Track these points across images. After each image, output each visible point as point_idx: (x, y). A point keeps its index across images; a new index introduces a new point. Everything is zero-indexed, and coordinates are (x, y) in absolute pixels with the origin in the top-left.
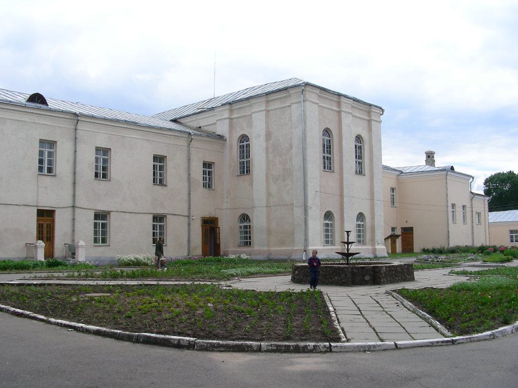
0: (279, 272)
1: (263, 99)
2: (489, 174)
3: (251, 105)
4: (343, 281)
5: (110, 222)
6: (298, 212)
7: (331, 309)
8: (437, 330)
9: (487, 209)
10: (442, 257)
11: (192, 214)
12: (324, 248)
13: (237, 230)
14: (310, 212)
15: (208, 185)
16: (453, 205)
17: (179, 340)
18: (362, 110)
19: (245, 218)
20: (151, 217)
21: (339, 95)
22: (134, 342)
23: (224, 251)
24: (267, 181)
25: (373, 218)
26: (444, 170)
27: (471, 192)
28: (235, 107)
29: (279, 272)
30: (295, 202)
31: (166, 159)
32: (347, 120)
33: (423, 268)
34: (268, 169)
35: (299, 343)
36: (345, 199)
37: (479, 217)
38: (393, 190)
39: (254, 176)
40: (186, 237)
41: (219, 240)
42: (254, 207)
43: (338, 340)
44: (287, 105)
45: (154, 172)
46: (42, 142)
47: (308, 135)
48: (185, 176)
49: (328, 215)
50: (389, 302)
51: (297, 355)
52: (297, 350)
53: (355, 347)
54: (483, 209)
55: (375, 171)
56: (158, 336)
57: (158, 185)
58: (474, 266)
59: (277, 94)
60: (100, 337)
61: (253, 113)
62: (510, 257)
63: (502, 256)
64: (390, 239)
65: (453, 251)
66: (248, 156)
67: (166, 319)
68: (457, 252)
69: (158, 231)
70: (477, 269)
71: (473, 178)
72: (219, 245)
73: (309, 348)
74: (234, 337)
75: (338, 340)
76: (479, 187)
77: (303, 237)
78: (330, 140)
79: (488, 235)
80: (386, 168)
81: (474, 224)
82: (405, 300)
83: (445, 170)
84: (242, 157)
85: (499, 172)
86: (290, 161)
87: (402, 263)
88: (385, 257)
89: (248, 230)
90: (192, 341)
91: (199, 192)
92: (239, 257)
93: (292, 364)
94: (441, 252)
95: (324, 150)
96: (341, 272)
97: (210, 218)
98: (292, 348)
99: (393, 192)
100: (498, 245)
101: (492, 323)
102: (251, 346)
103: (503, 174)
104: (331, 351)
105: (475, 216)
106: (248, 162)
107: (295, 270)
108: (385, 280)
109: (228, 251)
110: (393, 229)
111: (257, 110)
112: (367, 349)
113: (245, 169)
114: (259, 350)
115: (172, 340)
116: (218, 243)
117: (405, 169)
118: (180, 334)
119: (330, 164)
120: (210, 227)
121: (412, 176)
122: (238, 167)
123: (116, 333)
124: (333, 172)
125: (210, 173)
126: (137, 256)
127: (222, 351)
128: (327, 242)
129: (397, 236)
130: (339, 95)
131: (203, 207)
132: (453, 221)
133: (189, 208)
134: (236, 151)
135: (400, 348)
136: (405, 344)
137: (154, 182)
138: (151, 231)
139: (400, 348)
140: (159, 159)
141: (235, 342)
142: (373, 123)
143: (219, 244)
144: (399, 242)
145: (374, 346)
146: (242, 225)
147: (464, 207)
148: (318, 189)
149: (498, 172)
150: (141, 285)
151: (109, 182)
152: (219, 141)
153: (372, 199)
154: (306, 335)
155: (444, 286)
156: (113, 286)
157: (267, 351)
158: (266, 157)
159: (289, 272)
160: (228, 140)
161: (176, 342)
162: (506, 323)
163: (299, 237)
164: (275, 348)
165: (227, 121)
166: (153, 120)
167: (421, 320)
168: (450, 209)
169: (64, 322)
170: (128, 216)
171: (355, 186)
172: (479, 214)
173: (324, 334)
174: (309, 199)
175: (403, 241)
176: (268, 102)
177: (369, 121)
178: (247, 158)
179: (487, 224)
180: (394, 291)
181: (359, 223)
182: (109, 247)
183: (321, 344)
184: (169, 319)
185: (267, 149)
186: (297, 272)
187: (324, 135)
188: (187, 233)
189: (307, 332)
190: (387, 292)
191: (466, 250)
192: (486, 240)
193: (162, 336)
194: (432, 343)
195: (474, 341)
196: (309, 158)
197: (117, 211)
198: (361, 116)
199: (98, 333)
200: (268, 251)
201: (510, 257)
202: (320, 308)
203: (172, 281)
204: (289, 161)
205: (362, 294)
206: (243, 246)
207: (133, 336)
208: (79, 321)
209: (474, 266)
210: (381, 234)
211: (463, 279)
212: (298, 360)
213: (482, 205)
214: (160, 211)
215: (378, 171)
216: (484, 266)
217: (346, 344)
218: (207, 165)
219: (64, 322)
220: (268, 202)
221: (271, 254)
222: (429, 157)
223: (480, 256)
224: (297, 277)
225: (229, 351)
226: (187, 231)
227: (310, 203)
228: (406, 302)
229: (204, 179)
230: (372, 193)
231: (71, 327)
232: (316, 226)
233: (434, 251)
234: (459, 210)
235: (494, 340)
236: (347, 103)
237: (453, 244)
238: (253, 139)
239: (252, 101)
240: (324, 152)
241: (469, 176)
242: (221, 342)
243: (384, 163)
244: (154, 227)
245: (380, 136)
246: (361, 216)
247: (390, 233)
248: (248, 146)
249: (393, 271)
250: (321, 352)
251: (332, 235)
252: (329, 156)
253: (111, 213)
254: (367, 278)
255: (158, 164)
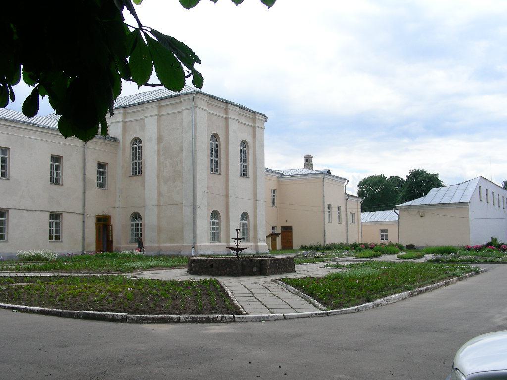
0: (175, 266)
1: (156, 105)
2: (362, 178)
3: (144, 110)
4: (234, 272)
5: (8, 218)
6: (187, 211)
7: (229, 292)
8: (315, 306)
9: (360, 210)
10: (319, 254)
11: (87, 211)
12: (210, 244)
13: (129, 228)
14: (198, 211)
15: (102, 184)
16: (329, 206)
17: (114, 315)
18: (247, 117)
19: (136, 216)
20: (48, 214)
21: (227, 103)
22: (75, 318)
23: (116, 247)
24: (159, 182)
25: (256, 217)
26: (321, 173)
27: (346, 194)
28: (129, 110)
29: (175, 266)
30: (184, 202)
31: (63, 158)
32: (233, 126)
33: (302, 263)
34: (159, 170)
35: (210, 316)
36: (231, 200)
37: (352, 217)
38: (274, 191)
39: (146, 176)
40: (81, 234)
41: (112, 237)
42: (145, 206)
43: (240, 313)
44: (179, 110)
45: (51, 172)
46: (382, 231)
47: (198, 140)
48: (81, 176)
49: (215, 214)
50: (273, 287)
51: (209, 324)
52: (208, 320)
53: (253, 318)
54: (356, 210)
55: (258, 174)
56: (96, 312)
57: (55, 184)
58: (347, 261)
59: (169, 100)
60: (44, 316)
61: (146, 117)
62: (379, 253)
63: (372, 252)
64: (271, 237)
65: (328, 248)
66: (140, 158)
67: (95, 301)
68: (333, 249)
69: (54, 228)
70: (349, 263)
71: (348, 181)
72: (112, 242)
73: (218, 319)
74: (158, 312)
75: (240, 313)
76: (353, 189)
77: (191, 235)
78: (217, 145)
79: (360, 233)
80: (268, 170)
81: (348, 223)
82: (288, 286)
83: (323, 173)
84: (134, 158)
85: (372, 175)
86: (181, 163)
87: (285, 257)
88: (267, 254)
89: (139, 227)
90: (124, 316)
91: (94, 191)
92: (132, 253)
93: (206, 329)
94: (318, 249)
95: (212, 154)
96: (232, 264)
97: (103, 216)
98: (204, 319)
99: (274, 193)
100: (369, 242)
101: (358, 301)
102: (172, 318)
103: (376, 177)
104: (234, 321)
105: (350, 217)
106: (140, 164)
107: (191, 263)
108: (270, 271)
109: (120, 247)
110: (274, 228)
111: (149, 115)
112: (262, 319)
113: (137, 170)
114: (179, 321)
115: (107, 316)
116: (111, 239)
117: (285, 172)
118: (112, 311)
119: (217, 167)
120: (103, 224)
121: (292, 178)
122: (130, 168)
123: (59, 312)
124: (220, 174)
125: (103, 173)
126: (37, 252)
127: (149, 323)
128: (214, 239)
129: (278, 234)
130: (227, 103)
131: (97, 205)
132: (329, 221)
133: (84, 207)
134: (129, 152)
135: (287, 319)
136: (292, 316)
137: (51, 181)
138: (47, 228)
139: (287, 319)
140: (56, 159)
141: (159, 316)
142: (257, 129)
143: (112, 241)
144: (279, 239)
145: (268, 317)
146: (134, 223)
147: (339, 208)
148: (206, 189)
149: (366, 176)
150: (56, 276)
151: (8, 181)
152: (111, 143)
153: (255, 200)
154: (214, 310)
155: (321, 276)
156: (31, 277)
157: (185, 322)
158: (158, 159)
159: (183, 265)
160: (121, 142)
161: (111, 317)
162: (368, 301)
163: (188, 234)
164: (191, 319)
165: (121, 124)
166: (48, 121)
167: (302, 299)
168: (326, 210)
169: (7, 305)
170: (25, 213)
171: (240, 187)
172: (353, 214)
173: (228, 309)
174: (198, 199)
175: (283, 239)
176: (160, 107)
177: (254, 128)
178: (139, 159)
179: (360, 222)
180: (279, 279)
181: (243, 221)
182: (8, 244)
183: (228, 316)
184: (97, 301)
185: (158, 151)
186: (193, 265)
187: (212, 139)
188: (82, 231)
189: (215, 308)
190: (273, 281)
191: (341, 247)
192: (359, 239)
193: (99, 313)
194: (312, 314)
195: (344, 313)
196: (198, 161)
197: (15, 209)
198: (248, 123)
199: (41, 312)
200: (159, 247)
201: (379, 253)
202: (220, 291)
203: (82, 273)
204: (179, 163)
205: (250, 281)
206: (134, 243)
207: (74, 313)
208: (21, 304)
209: (347, 261)
210: (263, 231)
211: (337, 270)
212: (214, 327)
213: (355, 206)
214: (56, 209)
215: (260, 173)
216: (356, 261)
217: (246, 315)
218: (101, 166)
219: (7, 305)
220: (158, 201)
221: (161, 250)
222: (307, 160)
223: (352, 252)
224: (194, 269)
225: (155, 323)
226: (82, 228)
227: (198, 203)
228: (289, 287)
229: (99, 179)
230: (255, 195)
231: (15, 309)
232: (204, 224)
233: (311, 248)
234: (334, 210)
235: (358, 313)
236: (234, 111)
237: (328, 242)
238: (146, 142)
239: (145, 106)
240: (212, 156)
241: (344, 179)
242: (148, 316)
243: (267, 166)
244: (51, 224)
245: (263, 141)
246: (245, 216)
247: (271, 231)
248: (140, 148)
249: (277, 263)
250: (227, 322)
251: (218, 233)
252: (216, 159)
253: (10, 210)
254: (255, 269)
255: (55, 164)
